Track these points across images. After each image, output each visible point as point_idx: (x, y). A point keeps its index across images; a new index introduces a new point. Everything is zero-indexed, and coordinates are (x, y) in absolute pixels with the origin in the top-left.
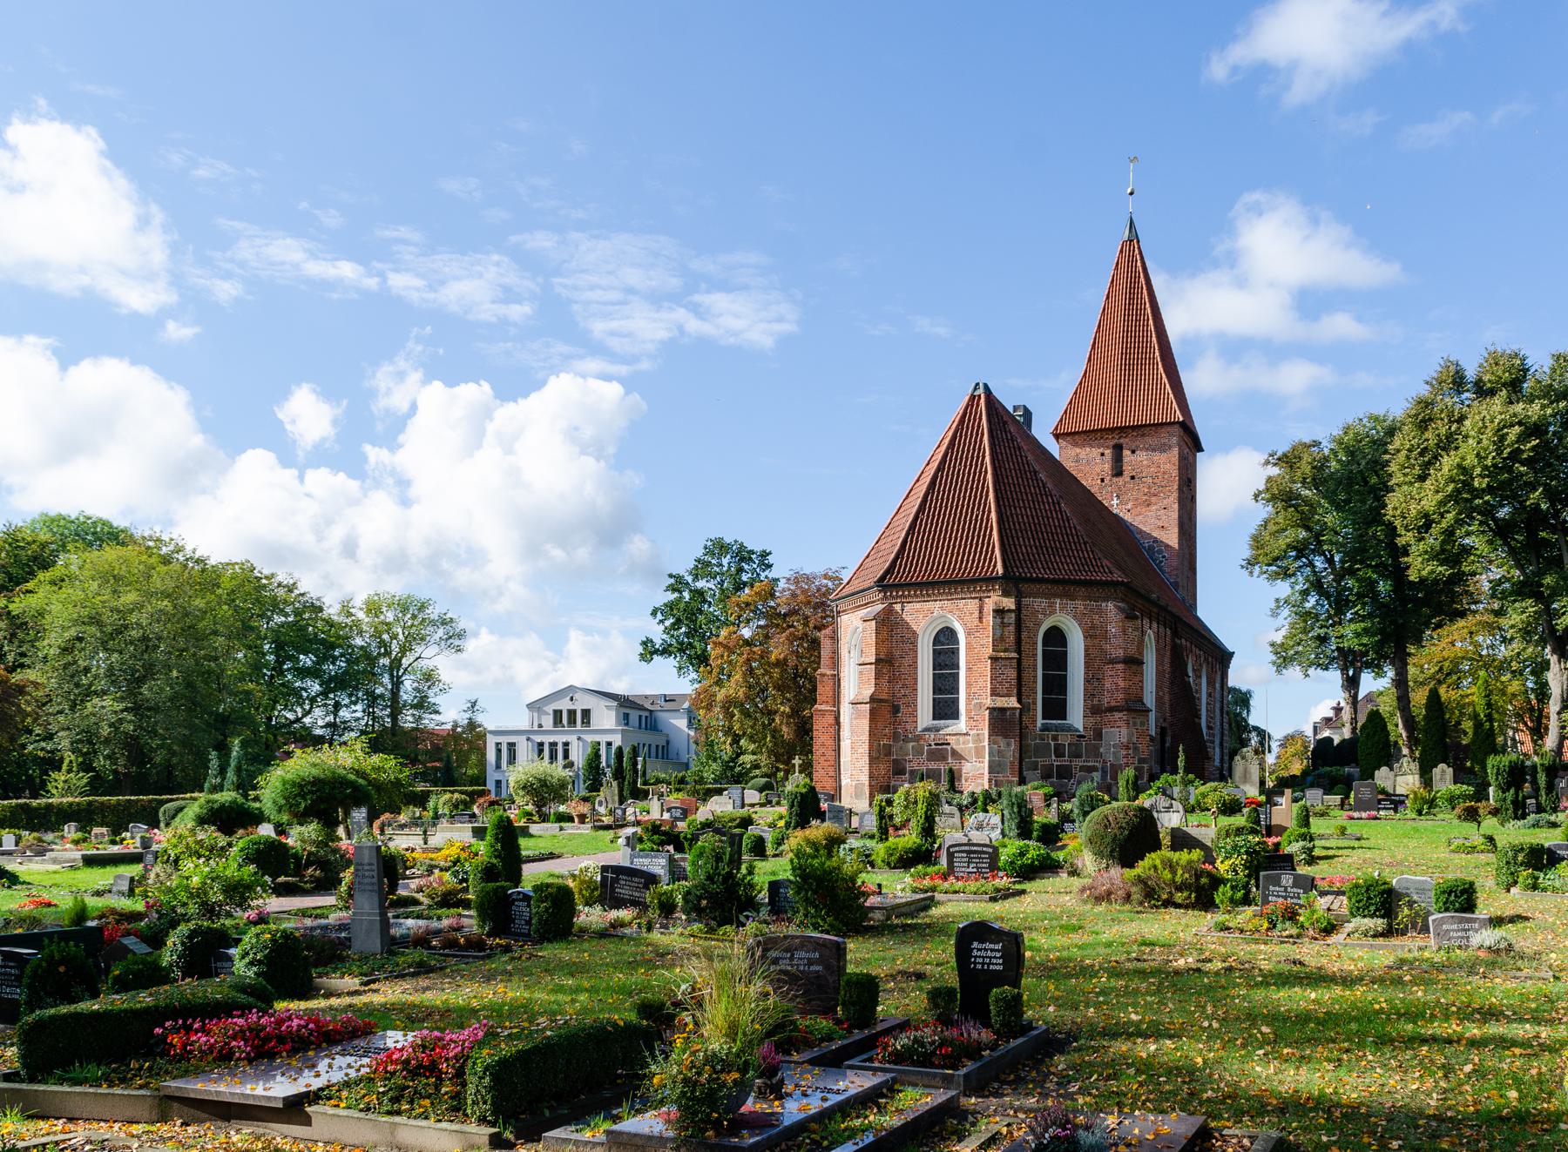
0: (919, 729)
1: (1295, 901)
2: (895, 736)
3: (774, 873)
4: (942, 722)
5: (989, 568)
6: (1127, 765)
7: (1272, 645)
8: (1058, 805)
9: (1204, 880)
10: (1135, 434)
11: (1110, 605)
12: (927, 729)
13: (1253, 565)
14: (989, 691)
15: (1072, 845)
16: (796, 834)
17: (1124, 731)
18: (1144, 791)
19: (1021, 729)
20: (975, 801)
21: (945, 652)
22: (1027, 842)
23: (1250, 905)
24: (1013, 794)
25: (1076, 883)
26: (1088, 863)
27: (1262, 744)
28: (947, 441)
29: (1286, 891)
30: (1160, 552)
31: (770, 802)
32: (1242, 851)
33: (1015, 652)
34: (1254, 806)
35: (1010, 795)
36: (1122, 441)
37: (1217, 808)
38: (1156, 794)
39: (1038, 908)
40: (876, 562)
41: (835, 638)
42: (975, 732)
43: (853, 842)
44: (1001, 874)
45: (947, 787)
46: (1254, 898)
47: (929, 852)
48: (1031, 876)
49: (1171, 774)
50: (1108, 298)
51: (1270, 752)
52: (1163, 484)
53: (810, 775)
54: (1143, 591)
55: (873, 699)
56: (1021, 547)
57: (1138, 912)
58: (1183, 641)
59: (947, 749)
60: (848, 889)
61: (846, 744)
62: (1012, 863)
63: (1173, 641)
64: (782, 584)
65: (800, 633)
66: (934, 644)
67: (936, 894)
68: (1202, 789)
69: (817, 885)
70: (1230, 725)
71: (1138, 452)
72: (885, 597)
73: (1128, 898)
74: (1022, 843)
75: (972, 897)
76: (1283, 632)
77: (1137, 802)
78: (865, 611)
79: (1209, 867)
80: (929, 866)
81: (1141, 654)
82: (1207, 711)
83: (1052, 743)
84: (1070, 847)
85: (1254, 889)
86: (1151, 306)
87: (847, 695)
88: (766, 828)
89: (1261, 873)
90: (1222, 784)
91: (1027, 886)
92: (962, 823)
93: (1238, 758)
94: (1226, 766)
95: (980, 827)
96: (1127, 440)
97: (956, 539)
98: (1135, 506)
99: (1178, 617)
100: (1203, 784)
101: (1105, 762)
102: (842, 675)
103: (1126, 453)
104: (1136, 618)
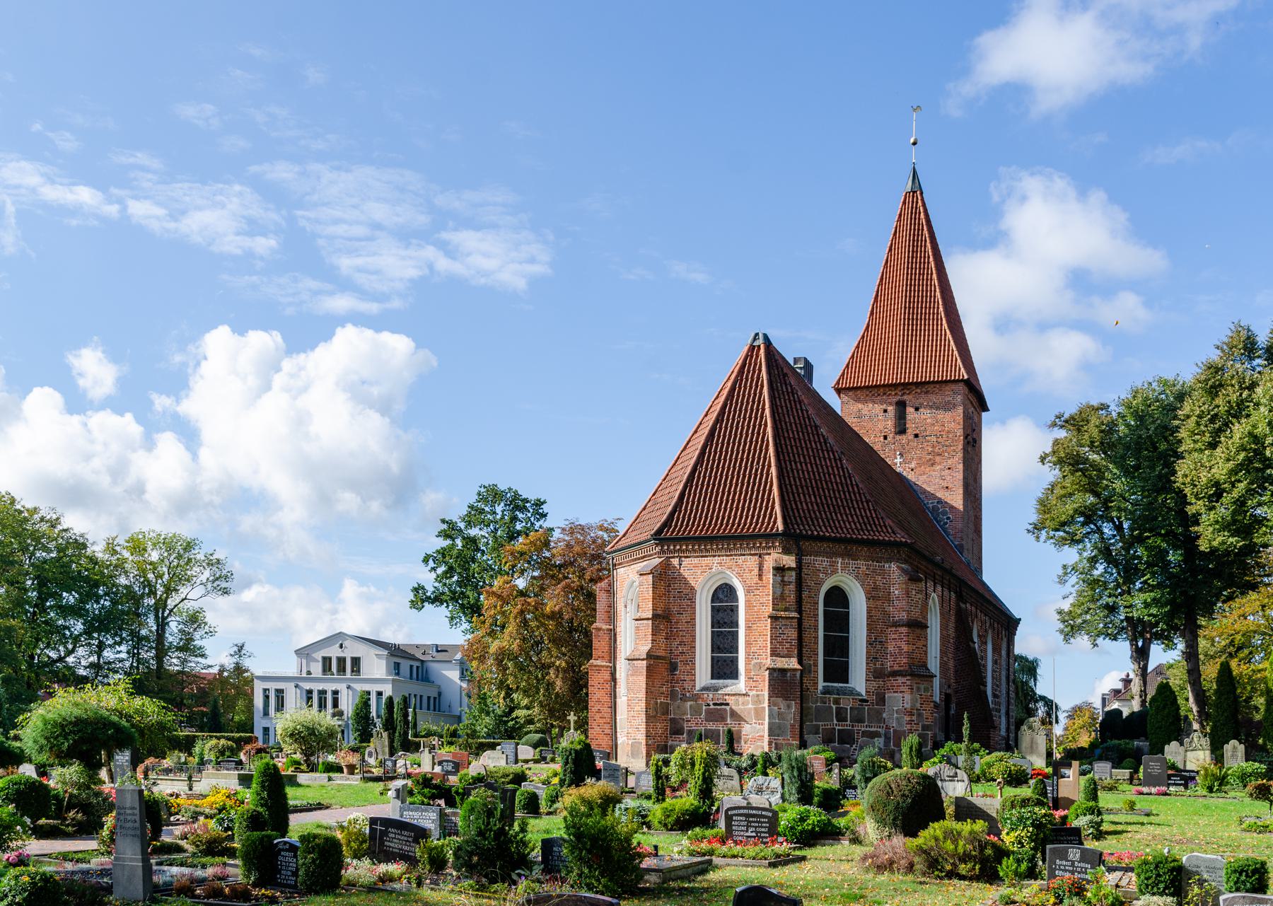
0: (698, 688)
1: (1083, 876)
2: (673, 695)
3: (547, 832)
4: (721, 681)
6: (911, 731)
7: (1060, 612)
8: (840, 771)
10: (919, 391)
11: (894, 566)
12: (705, 689)
14: (769, 651)
15: (854, 812)
16: (571, 792)
17: (908, 697)
18: (927, 759)
19: (801, 691)
20: (754, 764)
21: (723, 609)
23: (1036, 879)
24: (793, 757)
25: (858, 851)
26: (870, 831)
27: (1049, 714)
28: (725, 392)
29: (1073, 865)
30: (944, 513)
31: (544, 759)
33: (796, 611)
34: (1040, 777)
35: (790, 760)
36: (905, 397)
37: (1003, 778)
38: (941, 762)
40: (653, 514)
41: (610, 591)
42: (754, 692)
43: (630, 802)
44: (780, 839)
45: (726, 749)
46: (1040, 872)
48: (812, 842)
49: (956, 742)
51: (1057, 722)
52: (947, 443)
53: (585, 732)
55: (650, 656)
56: (801, 503)
57: (921, 883)
58: (968, 605)
59: (725, 710)
60: (623, 849)
61: (622, 701)
62: (792, 828)
63: (958, 605)
64: (557, 534)
66: (713, 601)
67: (714, 858)
68: (988, 759)
69: (591, 845)
70: (1017, 694)
71: (921, 410)
72: (662, 551)
73: (910, 868)
74: (802, 808)
75: (751, 862)
76: (1071, 600)
78: (645, 563)
79: (994, 839)
81: (925, 618)
83: (834, 707)
84: (851, 814)
85: (1041, 863)
88: (540, 785)
90: (1008, 754)
91: (807, 852)
93: (1024, 727)
94: (1012, 735)
95: (760, 791)
96: (910, 397)
99: (963, 581)
100: (988, 754)
101: (888, 728)
102: (618, 630)
103: (910, 410)
104: (919, 580)
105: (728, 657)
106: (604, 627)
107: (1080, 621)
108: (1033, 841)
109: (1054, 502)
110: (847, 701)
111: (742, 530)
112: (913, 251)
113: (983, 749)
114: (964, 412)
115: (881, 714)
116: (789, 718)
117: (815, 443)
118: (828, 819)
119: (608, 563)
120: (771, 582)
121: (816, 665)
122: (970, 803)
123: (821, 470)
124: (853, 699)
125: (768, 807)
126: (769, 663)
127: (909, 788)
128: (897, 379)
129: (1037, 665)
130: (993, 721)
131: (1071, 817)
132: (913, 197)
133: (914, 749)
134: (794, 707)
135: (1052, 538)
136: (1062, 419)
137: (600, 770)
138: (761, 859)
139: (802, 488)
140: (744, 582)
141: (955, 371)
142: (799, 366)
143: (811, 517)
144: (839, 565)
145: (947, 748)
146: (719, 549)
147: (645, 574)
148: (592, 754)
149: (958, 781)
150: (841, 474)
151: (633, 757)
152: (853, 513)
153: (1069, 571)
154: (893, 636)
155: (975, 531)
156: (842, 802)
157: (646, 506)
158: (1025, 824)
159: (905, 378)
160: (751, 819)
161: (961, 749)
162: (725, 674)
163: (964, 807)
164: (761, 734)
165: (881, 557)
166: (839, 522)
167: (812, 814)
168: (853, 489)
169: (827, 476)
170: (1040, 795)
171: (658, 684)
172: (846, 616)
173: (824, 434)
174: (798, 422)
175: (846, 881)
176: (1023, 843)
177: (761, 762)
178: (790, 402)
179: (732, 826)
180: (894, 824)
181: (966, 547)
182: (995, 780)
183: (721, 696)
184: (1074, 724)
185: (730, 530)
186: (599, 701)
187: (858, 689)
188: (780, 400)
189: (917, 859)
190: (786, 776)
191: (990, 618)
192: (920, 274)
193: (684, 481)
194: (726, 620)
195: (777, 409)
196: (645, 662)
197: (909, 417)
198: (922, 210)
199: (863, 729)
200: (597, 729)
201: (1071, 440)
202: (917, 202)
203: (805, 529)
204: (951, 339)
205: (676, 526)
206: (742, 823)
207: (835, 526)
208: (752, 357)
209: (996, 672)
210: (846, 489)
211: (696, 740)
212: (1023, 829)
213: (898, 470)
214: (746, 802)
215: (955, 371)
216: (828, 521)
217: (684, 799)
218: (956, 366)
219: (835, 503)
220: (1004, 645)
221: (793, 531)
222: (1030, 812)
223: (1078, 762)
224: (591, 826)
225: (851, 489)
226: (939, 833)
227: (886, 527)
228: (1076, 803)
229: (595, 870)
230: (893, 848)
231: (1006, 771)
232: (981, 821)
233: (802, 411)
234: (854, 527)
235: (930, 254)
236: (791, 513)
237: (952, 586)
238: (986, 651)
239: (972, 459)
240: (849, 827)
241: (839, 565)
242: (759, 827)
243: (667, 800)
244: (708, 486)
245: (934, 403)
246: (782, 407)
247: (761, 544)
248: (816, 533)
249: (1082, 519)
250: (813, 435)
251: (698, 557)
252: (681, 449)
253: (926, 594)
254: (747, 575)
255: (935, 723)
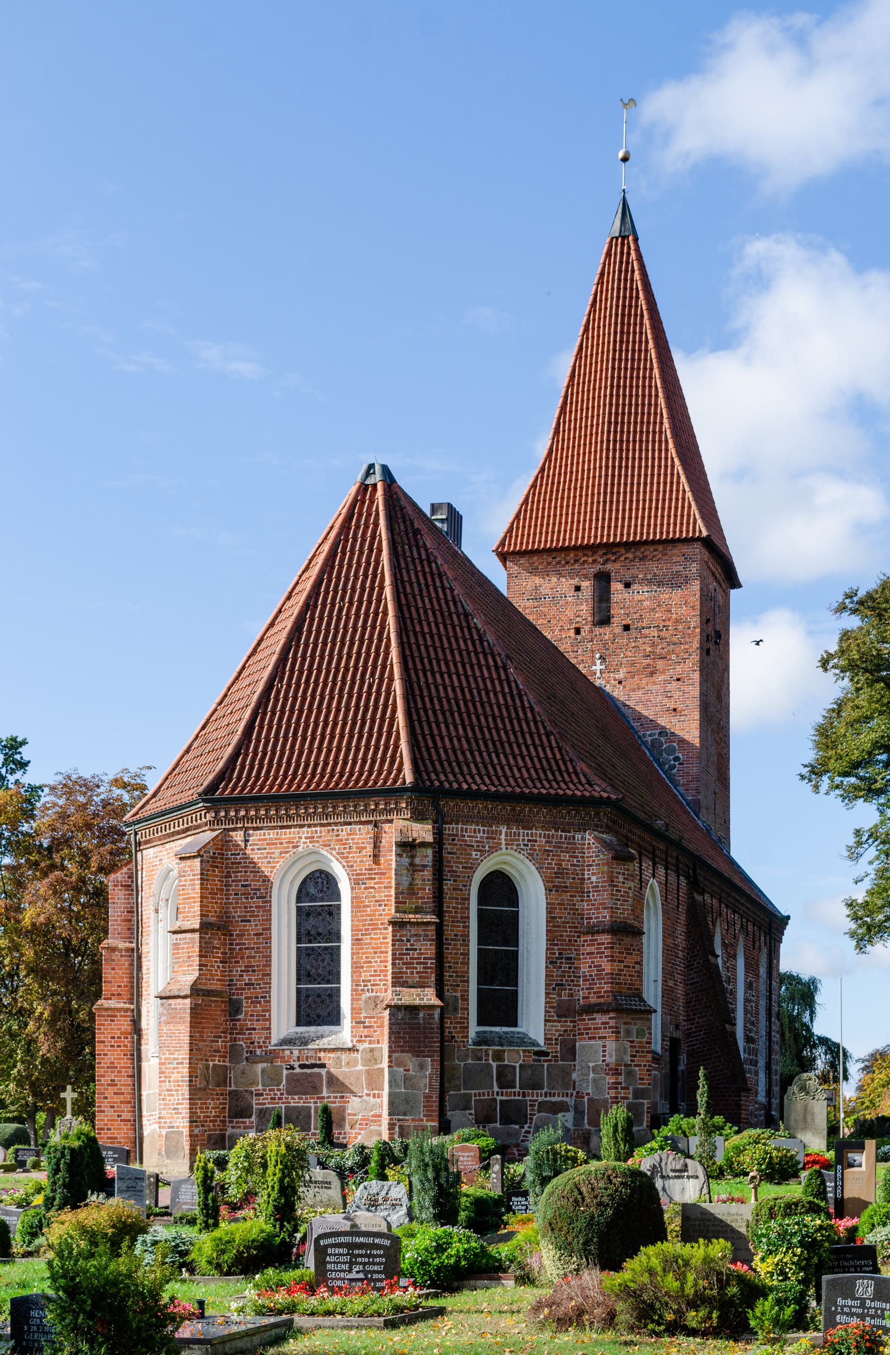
0: (274, 1040)
1: (877, 1322)
2: (234, 1053)
3: (23, 1285)
4: (312, 1029)
5: (389, 773)
6: (616, 1100)
7: (851, 905)
8: (503, 1167)
9: (733, 1290)
10: (630, 556)
11: (589, 837)
12: (287, 1041)
13: (819, 774)
14: (389, 977)
15: (523, 1233)
16: (63, 1217)
17: (611, 1045)
18: (641, 1144)
19: (442, 1041)
20: (366, 1161)
22: (447, 1228)
23: (806, 1330)
24: (426, 1149)
25: (529, 1295)
26: (547, 1262)
27: (833, 1065)
28: (320, 560)
29: (863, 1305)
30: (671, 751)
31: (21, 1164)
32: (795, 1241)
33: (433, 912)
34: (816, 1167)
35: (422, 1152)
36: (609, 566)
37: (758, 1170)
38: (662, 1148)
39: (464, 1339)
40: (202, 760)
41: (132, 887)
42: (366, 1045)
43: (161, 1231)
44: (403, 1282)
45: (320, 1138)
46: (813, 1318)
47: (286, 1247)
48: (455, 1284)
49: (687, 1115)
50: (586, 330)
51: (846, 1078)
52: (675, 639)
53: (91, 1118)
54: (641, 815)
55: (196, 991)
56: (442, 739)
57: (626, 1343)
58: (707, 897)
59: (320, 1075)
60: (146, 1309)
61: (150, 1066)
62: (423, 1263)
63: (690, 897)
64: (46, 798)
65: (74, 878)
66: (299, 899)
67: (296, 1317)
68: (736, 1140)
69: (94, 1304)
70: (782, 1035)
71: (635, 587)
72: (217, 820)
73: (610, 1320)
74: (440, 1231)
75: (355, 1321)
76: (867, 884)
77: (630, 1162)
78: (188, 840)
79: (741, 1268)
80: (286, 1270)
81: (639, 918)
82: (746, 1011)
83: (494, 1065)
84: (519, 1237)
85: (814, 1304)
86: (672, 418)
87: (151, 980)
88: (13, 1208)
89: (825, 1278)
90: (768, 1132)
91: (447, 1301)
92: (344, 1197)
93: (794, 1088)
94: (775, 1102)
95: (373, 1204)
96: (617, 565)
97: (335, 724)
98: (631, 674)
99: (699, 858)
100: (737, 1132)
101: (579, 1096)
102: (144, 949)
104: (630, 858)
105: (326, 989)
106: (122, 945)
107: (881, 917)
108: (801, 1269)
109: (843, 731)
110: (515, 1055)
111: (347, 783)
112: (622, 332)
113: (728, 1125)
114: (701, 589)
115: (569, 1074)
116: (422, 1085)
117: (465, 641)
118: (482, 1247)
119: (128, 842)
120: (394, 866)
121: (465, 999)
122: (705, 1213)
123: (473, 686)
124: (524, 1051)
125: (386, 1231)
126: (390, 997)
127: (609, 1192)
128: (596, 537)
129: (816, 988)
130: (745, 1080)
131: (864, 1229)
132: (623, 244)
133: (620, 1129)
134: (430, 1067)
135: (837, 787)
136: (855, 599)
137: (113, 1179)
138: (372, 1316)
139: (444, 714)
140: (349, 867)
141: (688, 524)
142: (440, 517)
143: (457, 760)
144: (503, 837)
145: (672, 1125)
146: (309, 815)
147: (189, 858)
148: (100, 1154)
149: (688, 1177)
150: (507, 690)
151: (168, 1157)
152: (525, 753)
153: (864, 839)
154: (589, 949)
155: (718, 779)
156: (505, 1218)
157: (190, 746)
158: (790, 1243)
159: (615, 535)
160: (356, 1252)
161: (694, 1127)
162: (319, 1016)
163: (695, 1220)
164: (377, 1112)
165: (568, 824)
166: (502, 768)
167: (456, 1239)
168: (525, 714)
169: (483, 693)
170: (816, 1196)
171: (208, 1035)
172: (514, 918)
173: (480, 626)
174: (437, 607)
175: (507, 1345)
176: (786, 1273)
177: (376, 1158)
178: (424, 575)
179: (325, 1263)
180: (585, 1250)
181: (703, 803)
182: (747, 1174)
183: (311, 1054)
184: (873, 1080)
185: (328, 784)
186: (112, 1067)
187: (532, 1035)
188: (408, 572)
189: (620, 1306)
190: (415, 1180)
191: (742, 917)
192: (632, 369)
193: (253, 705)
194: (320, 930)
195: (404, 588)
196: (188, 1001)
197: (615, 598)
198: (636, 267)
199: (540, 1099)
200: (110, 1112)
201: (868, 631)
202: (629, 254)
203: (447, 780)
204: (681, 472)
205: (239, 778)
206: (342, 1259)
207: (497, 775)
208: (363, 502)
209: (750, 1001)
210: (514, 715)
211: (270, 1125)
212: (787, 1251)
213: (598, 683)
214: (349, 1223)
215: (688, 524)
216: (485, 767)
217: (249, 1223)
218: (689, 515)
219: (496, 738)
220: (764, 960)
221: (428, 783)
222: (797, 1223)
223: (874, 1141)
224: (93, 1274)
225: (521, 715)
226: (655, 1262)
227: (577, 775)
228: (870, 1207)
229: (100, 1345)
230: (583, 1289)
231: (764, 1159)
232: (722, 1240)
233: (443, 589)
234: (526, 775)
235: (649, 337)
236: (425, 754)
237: (681, 866)
238: (734, 968)
239: (714, 663)
240: (515, 1258)
241: (503, 837)
242: (369, 1263)
243: (222, 1224)
244: (292, 712)
245: (655, 575)
246: (411, 584)
247: (377, 805)
248: (465, 786)
249: (884, 757)
250: (462, 629)
251: (274, 828)
252: (248, 653)
253: (641, 880)
254: (354, 856)
255: (655, 1087)
